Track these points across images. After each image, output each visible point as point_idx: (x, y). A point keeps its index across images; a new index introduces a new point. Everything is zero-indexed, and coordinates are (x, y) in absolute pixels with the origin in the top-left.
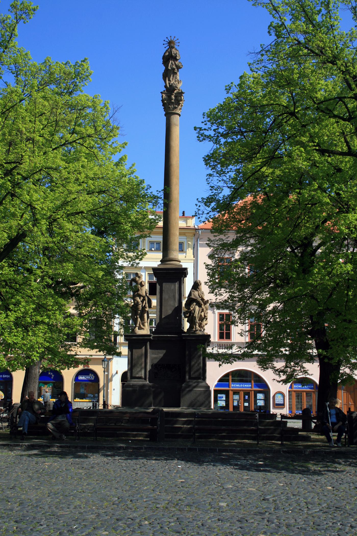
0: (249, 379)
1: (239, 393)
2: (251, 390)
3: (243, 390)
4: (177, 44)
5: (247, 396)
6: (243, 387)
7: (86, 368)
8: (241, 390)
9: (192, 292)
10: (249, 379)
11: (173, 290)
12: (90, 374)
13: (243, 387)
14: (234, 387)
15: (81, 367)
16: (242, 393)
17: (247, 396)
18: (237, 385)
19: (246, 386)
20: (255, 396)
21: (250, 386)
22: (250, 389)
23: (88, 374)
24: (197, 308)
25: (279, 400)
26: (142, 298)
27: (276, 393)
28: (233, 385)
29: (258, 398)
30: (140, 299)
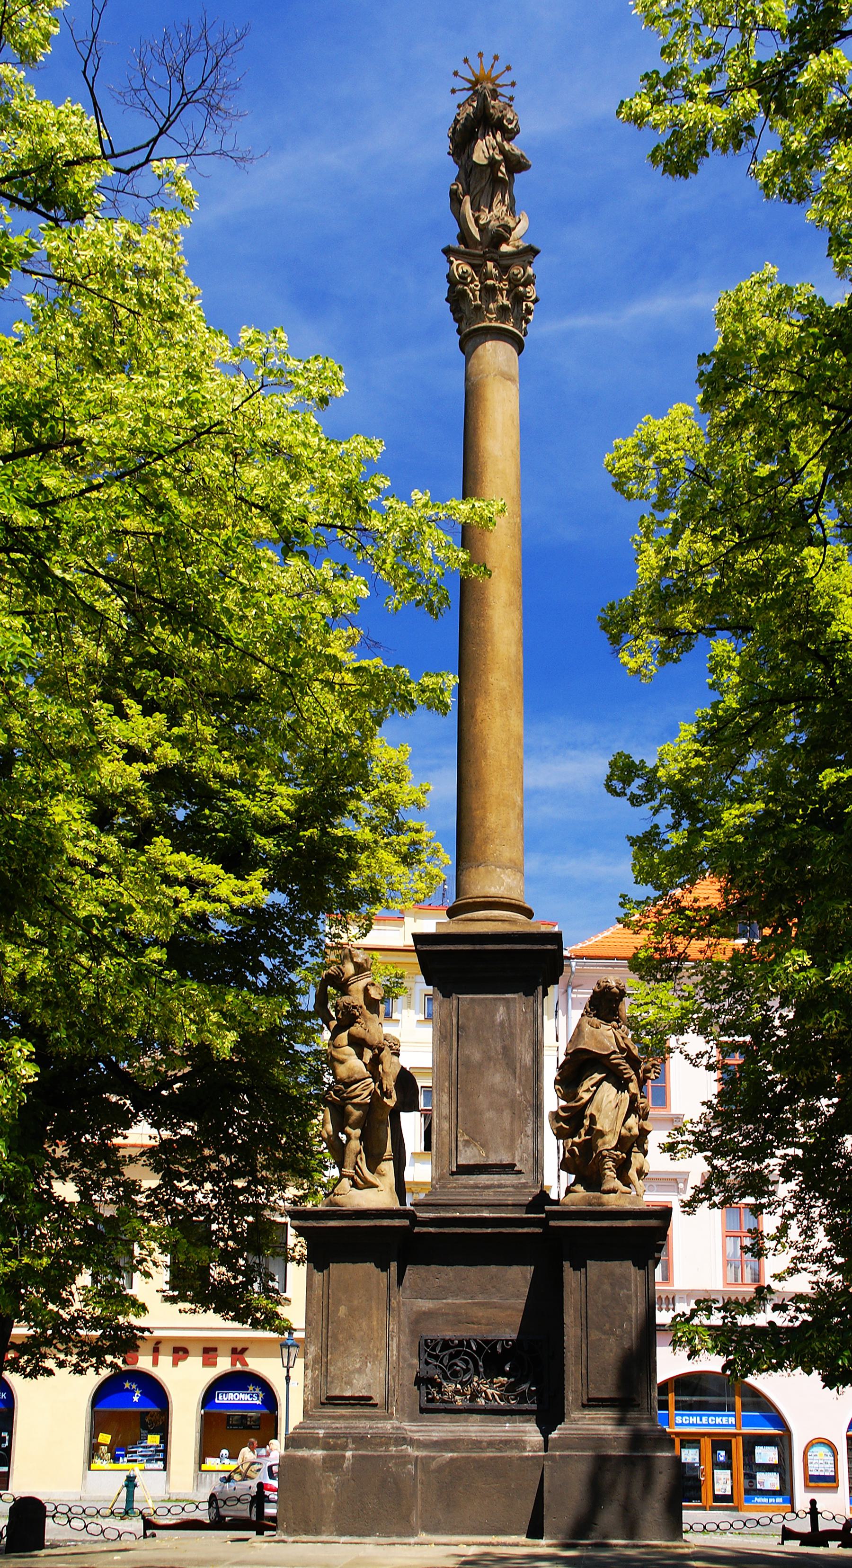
0: (726, 1399)
1: (699, 1441)
2: (735, 1435)
3: (709, 1435)
4: (500, 67)
5: (723, 1453)
6: (709, 1425)
7: (239, 1367)
8: (704, 1435)
9: (587, 1028)
10: (726, 1399)
11: (502, 1023)
12: (251, 1388)
13: (709, 1425)
14: (682, 1424)
15: (224, 1365)
16: (706, 1443)
17: (723, 1453)
18: (693, 1420)
19: (718, 1420)
20: (749, 1454)
21: (732, 1420)
22: (733, 1430)
23: (243, 1388)
24: (608, 1090)
25: (820, 1463)
26: (368, 1054)
27: (810, 1445)
28: (678, 1420)
29: (759, 1459)
30: (360, 1056)
